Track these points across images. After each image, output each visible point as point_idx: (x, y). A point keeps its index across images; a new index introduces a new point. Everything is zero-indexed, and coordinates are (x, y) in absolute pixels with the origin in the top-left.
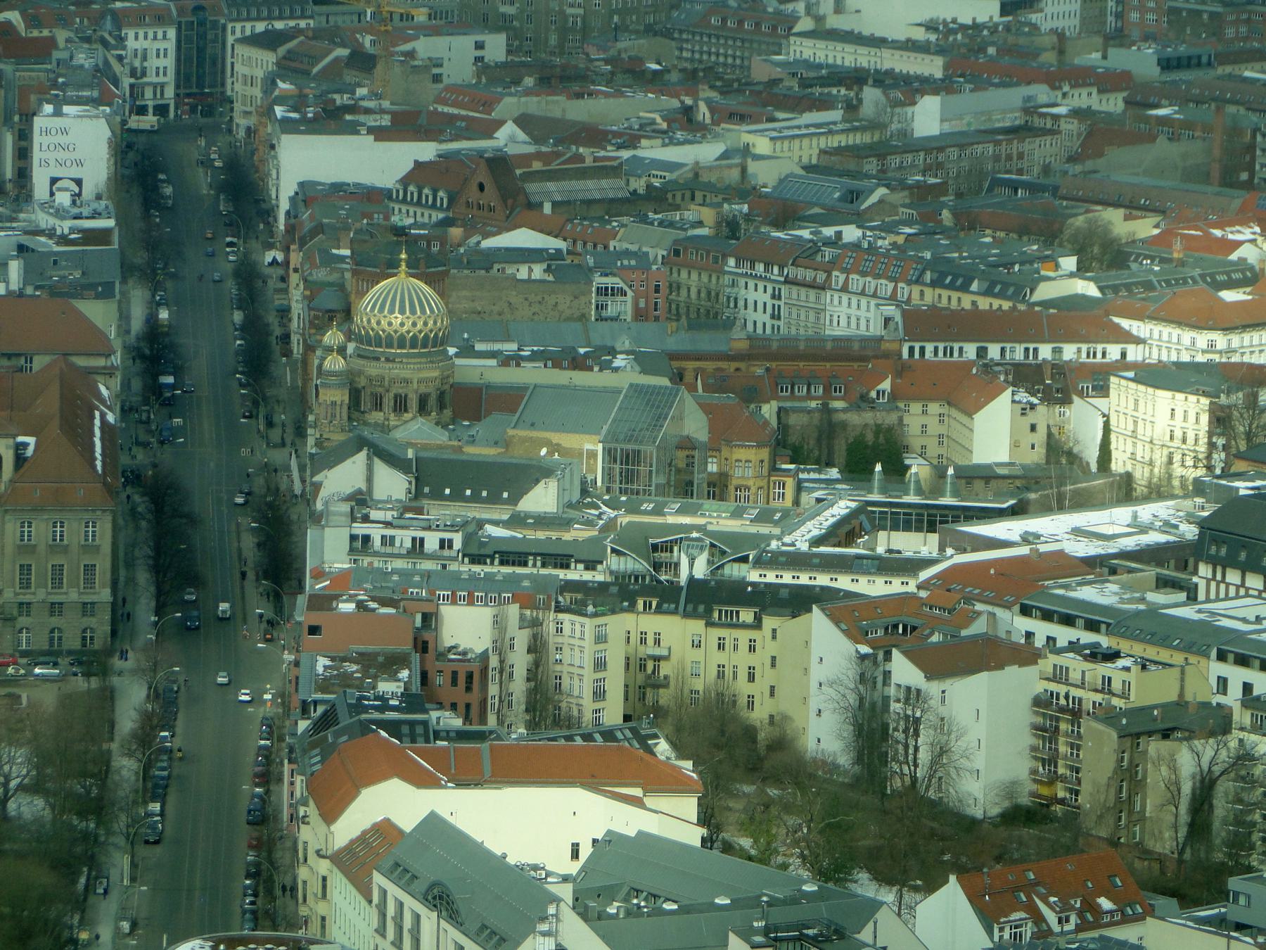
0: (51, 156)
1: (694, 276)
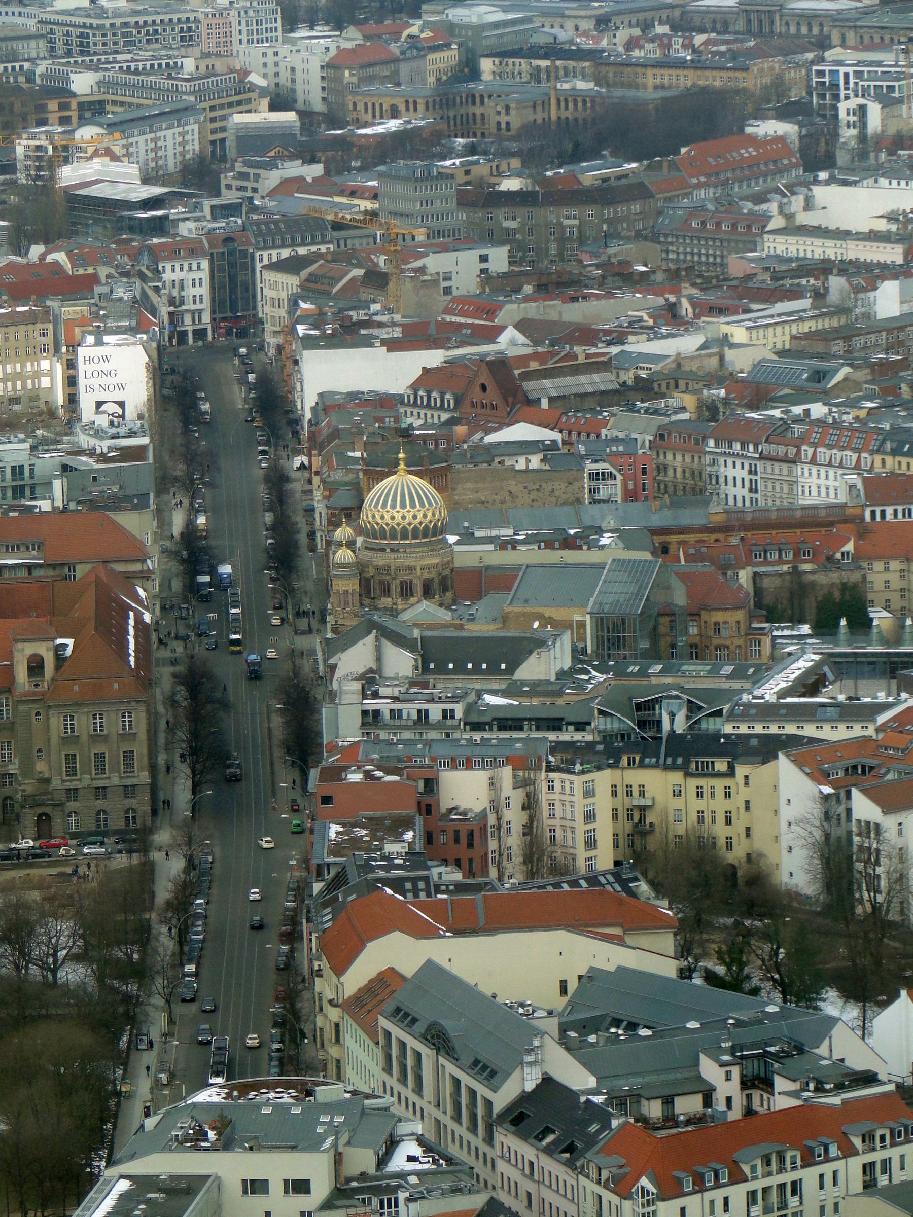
0: (95, 382)
1: (679, 458)
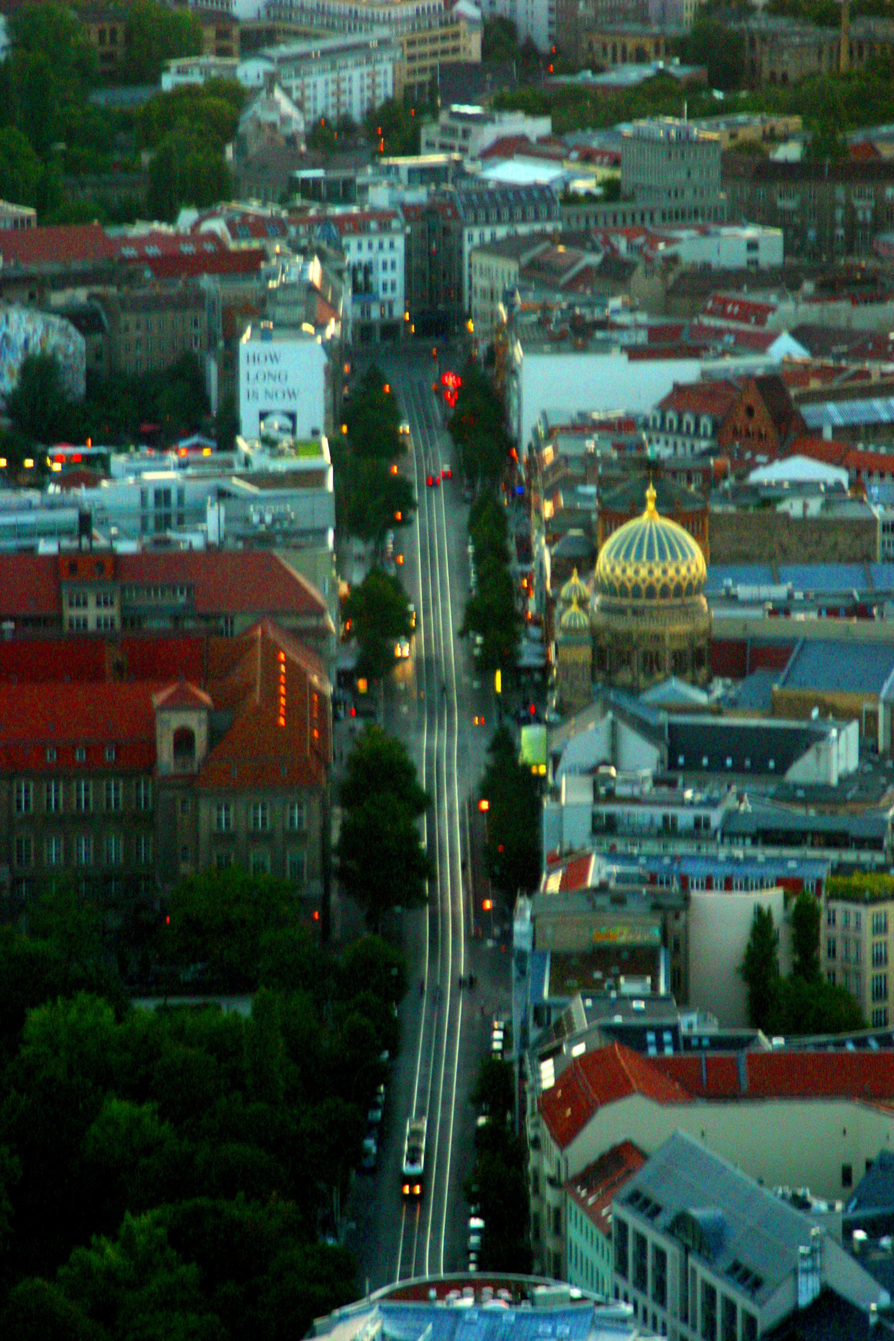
0: (261, 387)
